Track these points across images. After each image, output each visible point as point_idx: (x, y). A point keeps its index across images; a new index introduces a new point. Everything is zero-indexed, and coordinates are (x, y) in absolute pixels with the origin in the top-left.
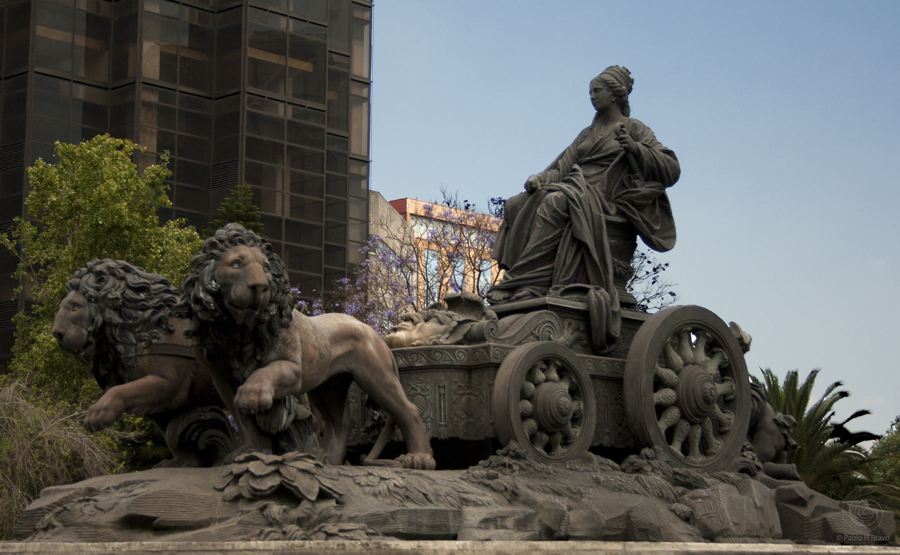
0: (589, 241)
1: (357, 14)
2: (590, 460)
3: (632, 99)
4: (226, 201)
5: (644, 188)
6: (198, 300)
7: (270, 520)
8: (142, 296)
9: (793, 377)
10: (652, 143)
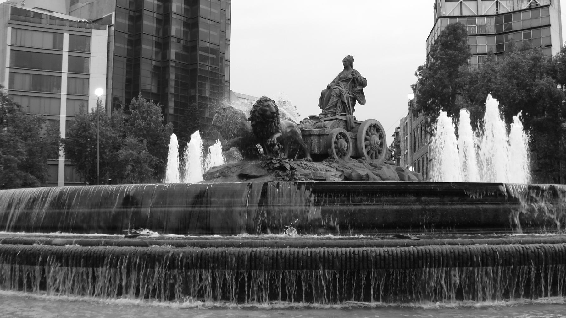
0: (346, 102)
1: (227, 42)
3: (354, 64)
5: (359, 88)
7: (476, 148)
10: (360, 76)
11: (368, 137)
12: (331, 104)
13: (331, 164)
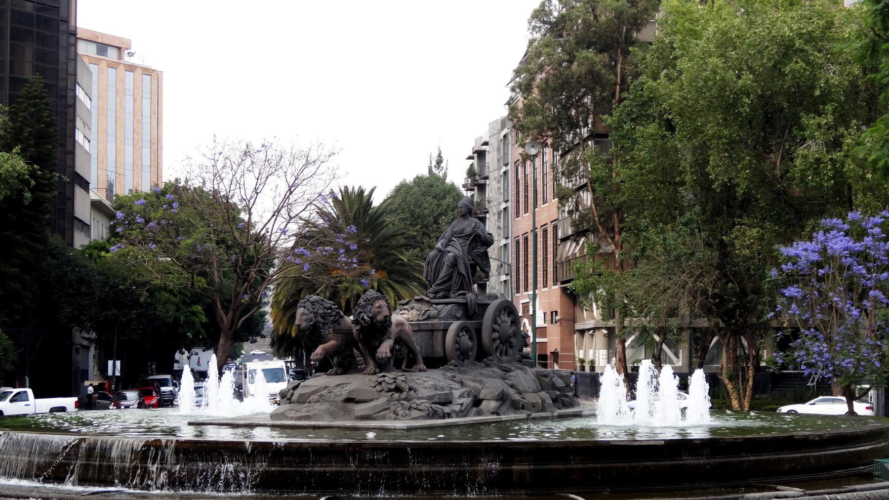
2: (476, 364)
4: (26, 86)
6: (363, 319)
8: (329, 311)
9: (361, 192)
11: (496, 326)
12: (444, 277)
13: (455, 377)
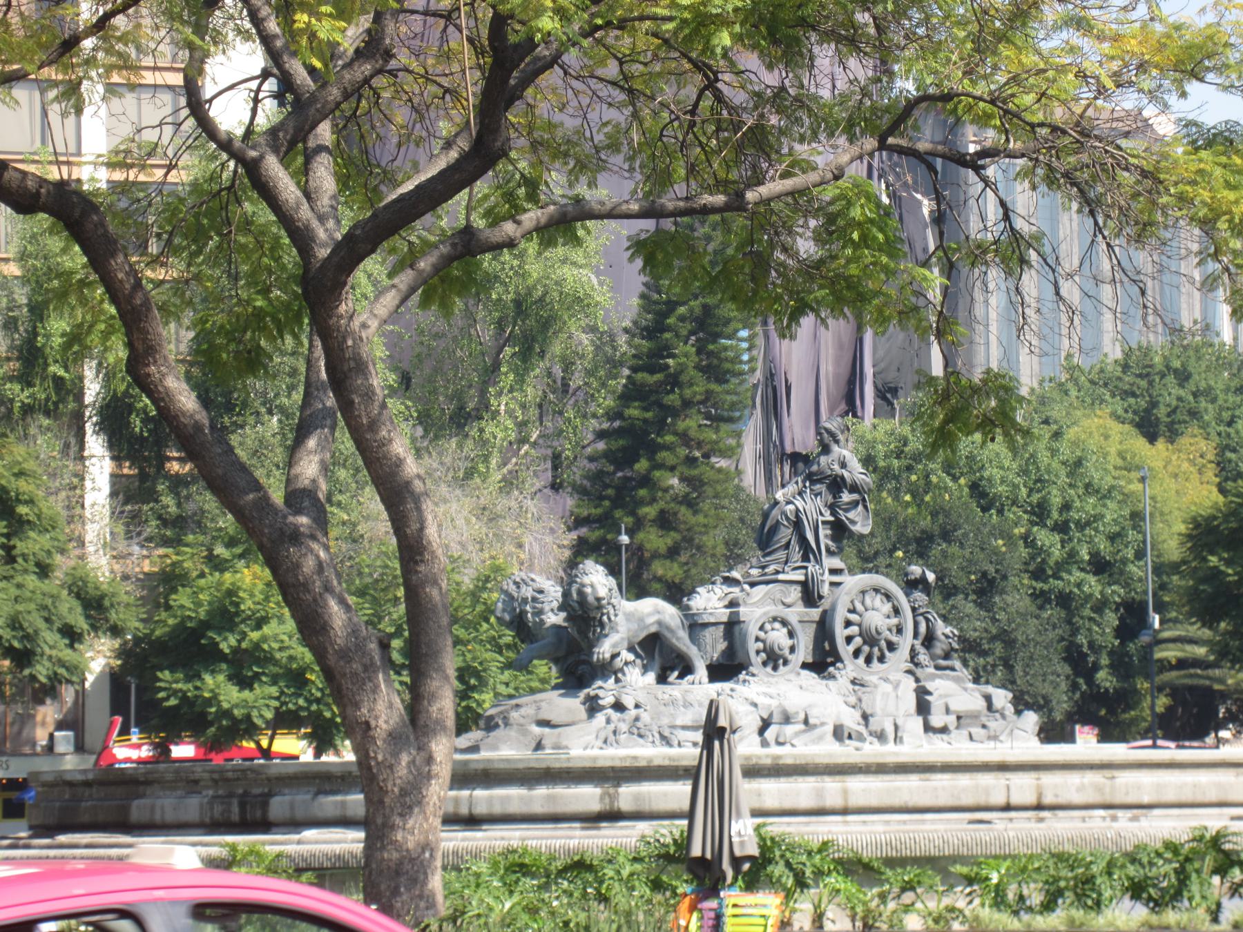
2: (799, 674)
